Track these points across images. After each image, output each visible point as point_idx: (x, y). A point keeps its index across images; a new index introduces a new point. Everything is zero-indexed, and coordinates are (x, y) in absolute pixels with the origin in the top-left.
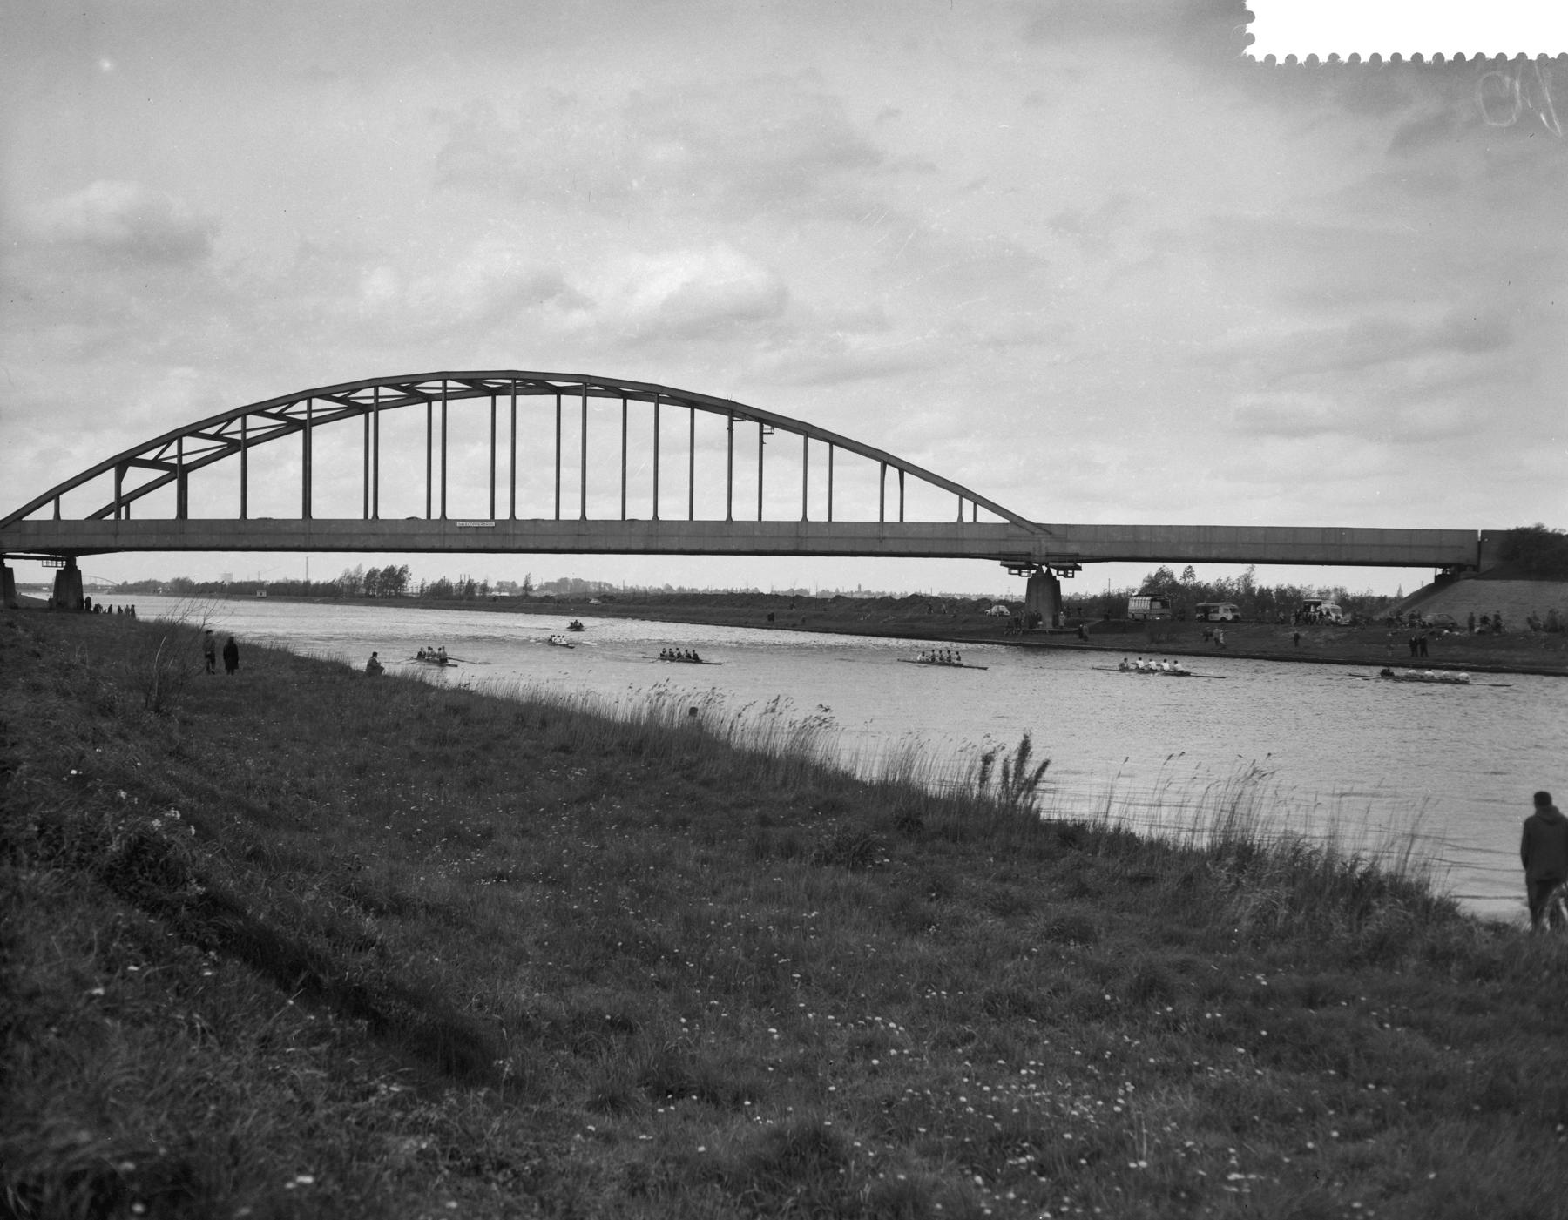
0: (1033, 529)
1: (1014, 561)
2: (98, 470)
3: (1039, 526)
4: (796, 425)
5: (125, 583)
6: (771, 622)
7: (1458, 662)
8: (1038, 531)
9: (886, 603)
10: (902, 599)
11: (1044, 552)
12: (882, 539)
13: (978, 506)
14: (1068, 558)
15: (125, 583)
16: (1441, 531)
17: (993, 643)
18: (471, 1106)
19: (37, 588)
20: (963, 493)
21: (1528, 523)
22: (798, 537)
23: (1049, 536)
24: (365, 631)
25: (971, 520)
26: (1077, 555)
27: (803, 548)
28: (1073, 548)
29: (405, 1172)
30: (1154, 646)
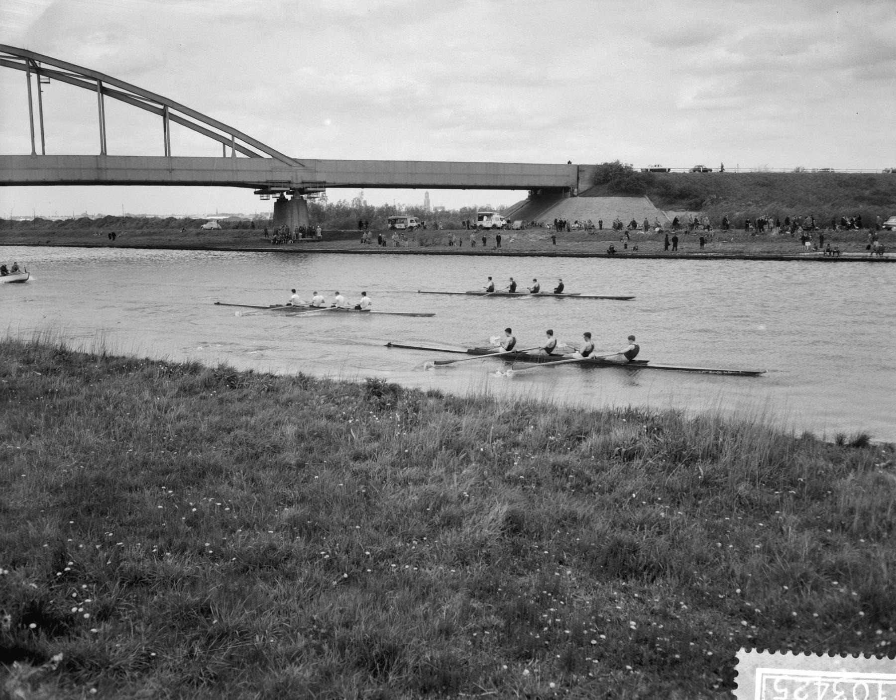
0: (290, 162)
1: (264, 189)
2: (208, 133)
3: (295, 160)
4: (61, 77)
5: (387, 205)
6: (112, 241)
7: (693, 253)
8: (294, 164)
9: (85, 222)
10: (98, 220)
11: (300, 181)
12: (171, 170)
13: (226, 146)
14: (318, 185)
15: (387, 205)
16: (337, 162)
17: (241, 250)
18: (822, 463)
19: (267, 214)
20: (236, 134)
21: (610, 160)
22: (98, 169)
23: (302, 168)
24: (192, 243)
25: (41, 153)
26: (325, 182)
27: (104, 178)
28: (320, 178)
29: (39, 680)
30: (423, 249)
